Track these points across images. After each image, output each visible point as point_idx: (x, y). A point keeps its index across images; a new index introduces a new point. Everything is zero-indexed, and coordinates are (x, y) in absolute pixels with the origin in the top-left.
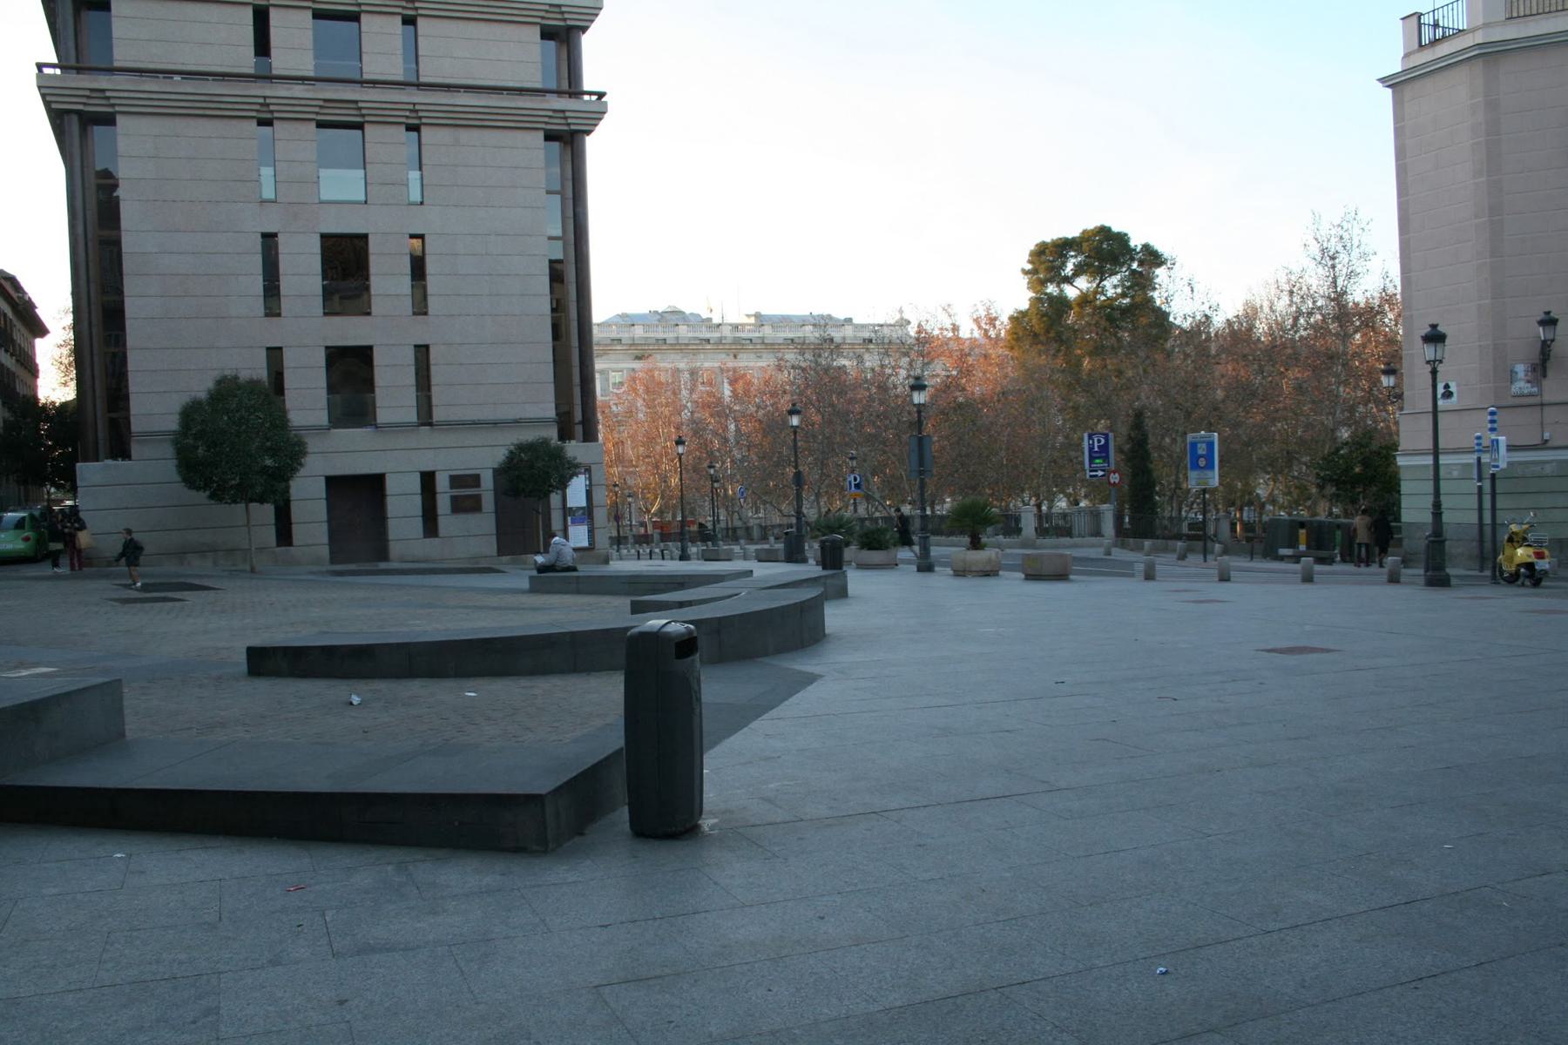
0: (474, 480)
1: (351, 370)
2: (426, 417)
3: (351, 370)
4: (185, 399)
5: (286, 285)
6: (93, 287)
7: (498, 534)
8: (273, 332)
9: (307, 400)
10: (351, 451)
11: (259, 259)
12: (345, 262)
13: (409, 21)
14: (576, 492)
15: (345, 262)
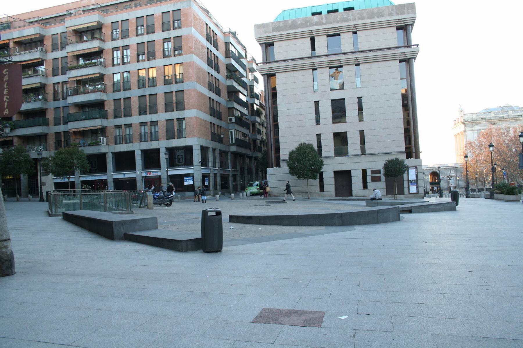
0: (378, 172)
1: (341, 139)
2: (363, 152)
3: (341, 139)
4: (290, 150)
5: (322, 115)
6: (271, 120)
7: (386, 188)
8: (318, 130)
9: (328, 147)
10: (342, 164)
11: (314, 109)
12: (339, 109)
13: (355, 33)
14: (412, 174)
15: (339, 109)
